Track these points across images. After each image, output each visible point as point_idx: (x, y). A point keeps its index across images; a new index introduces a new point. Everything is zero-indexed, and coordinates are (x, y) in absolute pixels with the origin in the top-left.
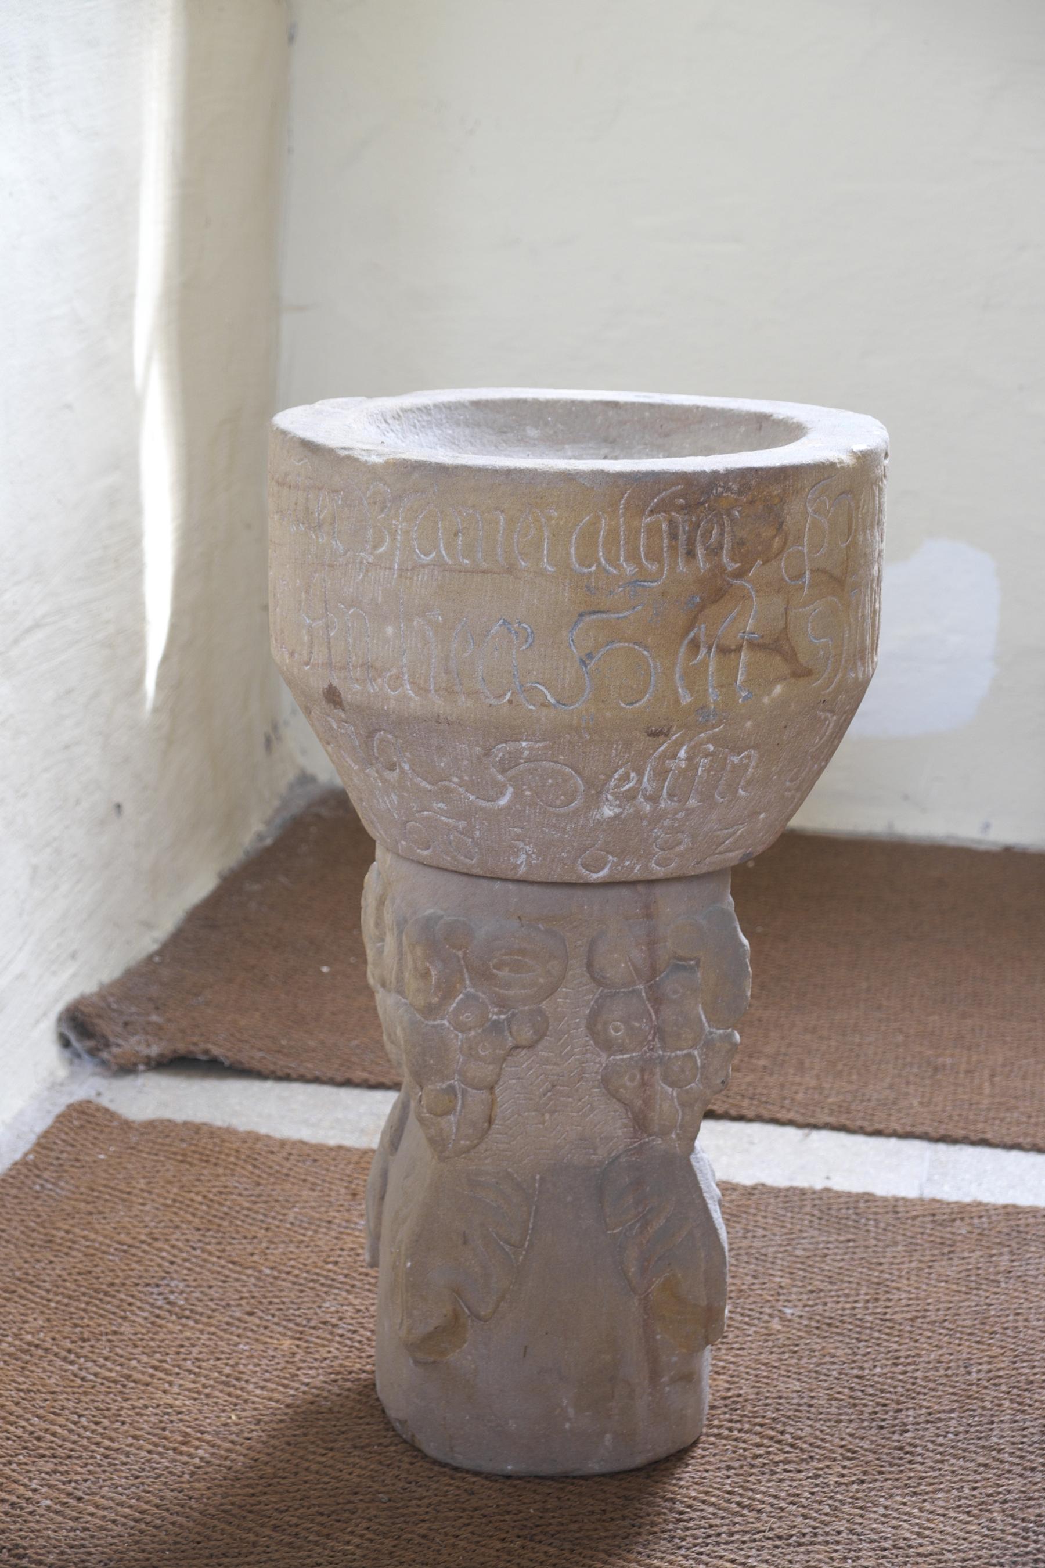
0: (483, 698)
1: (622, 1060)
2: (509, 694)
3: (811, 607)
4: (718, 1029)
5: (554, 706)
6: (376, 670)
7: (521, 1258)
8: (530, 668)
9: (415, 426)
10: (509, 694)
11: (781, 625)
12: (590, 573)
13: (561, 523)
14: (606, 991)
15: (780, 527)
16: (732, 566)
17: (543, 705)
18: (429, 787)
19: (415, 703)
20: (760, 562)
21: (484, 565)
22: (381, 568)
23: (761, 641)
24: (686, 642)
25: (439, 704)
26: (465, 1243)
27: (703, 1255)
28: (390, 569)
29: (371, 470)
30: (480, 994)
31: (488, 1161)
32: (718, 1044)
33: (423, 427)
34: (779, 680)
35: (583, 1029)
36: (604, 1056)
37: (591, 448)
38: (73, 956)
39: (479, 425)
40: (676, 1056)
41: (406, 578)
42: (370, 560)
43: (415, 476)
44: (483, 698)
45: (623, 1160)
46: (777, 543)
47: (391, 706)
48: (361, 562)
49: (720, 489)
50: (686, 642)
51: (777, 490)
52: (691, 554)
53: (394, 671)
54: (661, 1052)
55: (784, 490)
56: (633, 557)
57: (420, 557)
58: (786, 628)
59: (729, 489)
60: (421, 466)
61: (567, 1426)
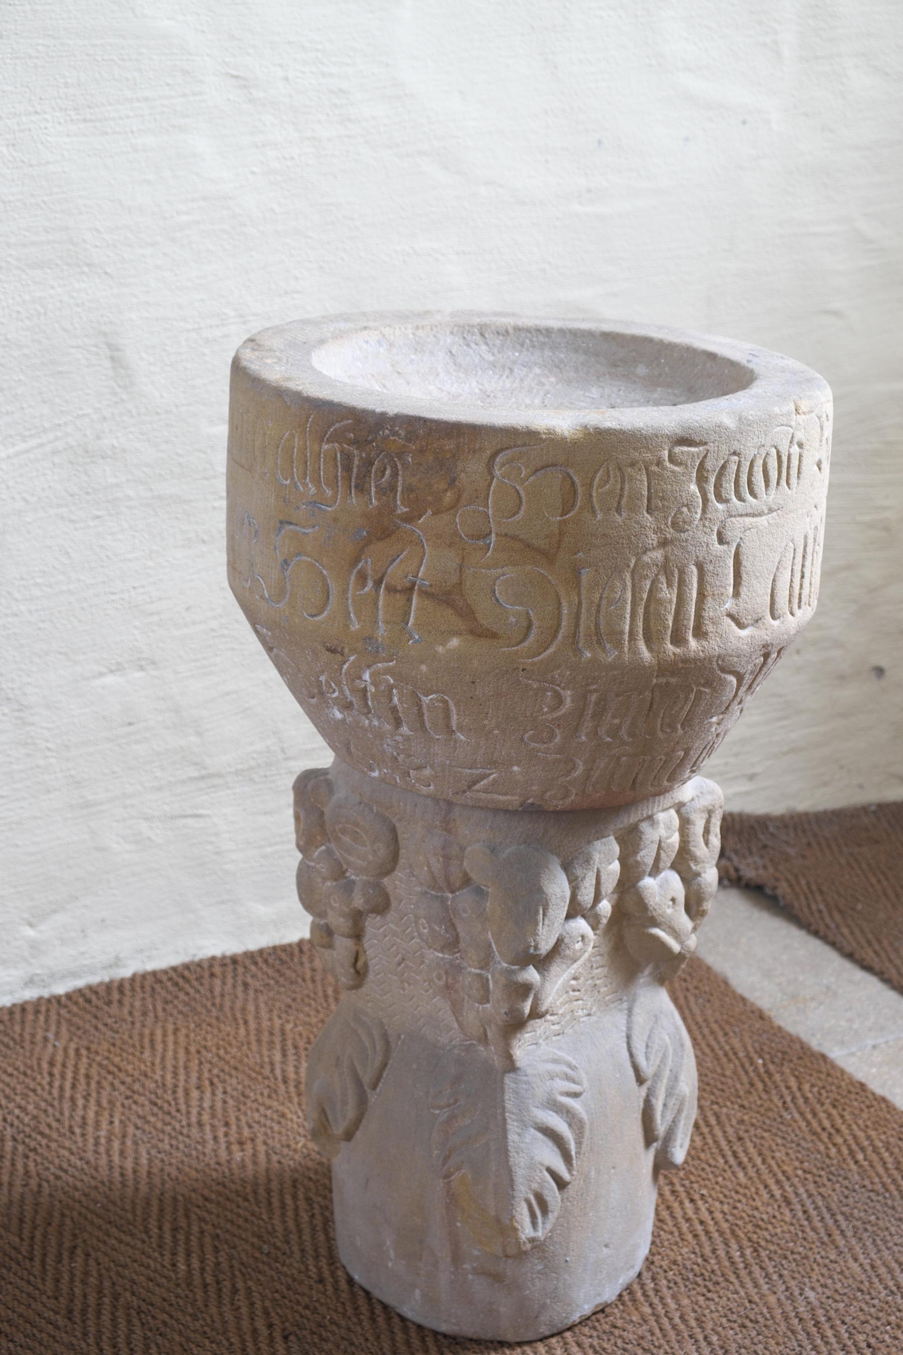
3: (500, 571)
9: (522, 345)
11: (454, 579)
15: (452, 482)
16: (402, 509)
20: (429, 512)
23: (429, 589)
24: (355, 571)
27: (494, 1169)
33: (534, 347)
34: (458, 633)
38: (751, 777)
39: (597, 355)
45: (456, 1051)
46: (449, 497)
49: (387, 432)
50: (355, 571)
51: (450, 445)
52: (362, 488)
55: (458, 447)
56: (317, 481)
58: (460, 584)
59: (396, 434)
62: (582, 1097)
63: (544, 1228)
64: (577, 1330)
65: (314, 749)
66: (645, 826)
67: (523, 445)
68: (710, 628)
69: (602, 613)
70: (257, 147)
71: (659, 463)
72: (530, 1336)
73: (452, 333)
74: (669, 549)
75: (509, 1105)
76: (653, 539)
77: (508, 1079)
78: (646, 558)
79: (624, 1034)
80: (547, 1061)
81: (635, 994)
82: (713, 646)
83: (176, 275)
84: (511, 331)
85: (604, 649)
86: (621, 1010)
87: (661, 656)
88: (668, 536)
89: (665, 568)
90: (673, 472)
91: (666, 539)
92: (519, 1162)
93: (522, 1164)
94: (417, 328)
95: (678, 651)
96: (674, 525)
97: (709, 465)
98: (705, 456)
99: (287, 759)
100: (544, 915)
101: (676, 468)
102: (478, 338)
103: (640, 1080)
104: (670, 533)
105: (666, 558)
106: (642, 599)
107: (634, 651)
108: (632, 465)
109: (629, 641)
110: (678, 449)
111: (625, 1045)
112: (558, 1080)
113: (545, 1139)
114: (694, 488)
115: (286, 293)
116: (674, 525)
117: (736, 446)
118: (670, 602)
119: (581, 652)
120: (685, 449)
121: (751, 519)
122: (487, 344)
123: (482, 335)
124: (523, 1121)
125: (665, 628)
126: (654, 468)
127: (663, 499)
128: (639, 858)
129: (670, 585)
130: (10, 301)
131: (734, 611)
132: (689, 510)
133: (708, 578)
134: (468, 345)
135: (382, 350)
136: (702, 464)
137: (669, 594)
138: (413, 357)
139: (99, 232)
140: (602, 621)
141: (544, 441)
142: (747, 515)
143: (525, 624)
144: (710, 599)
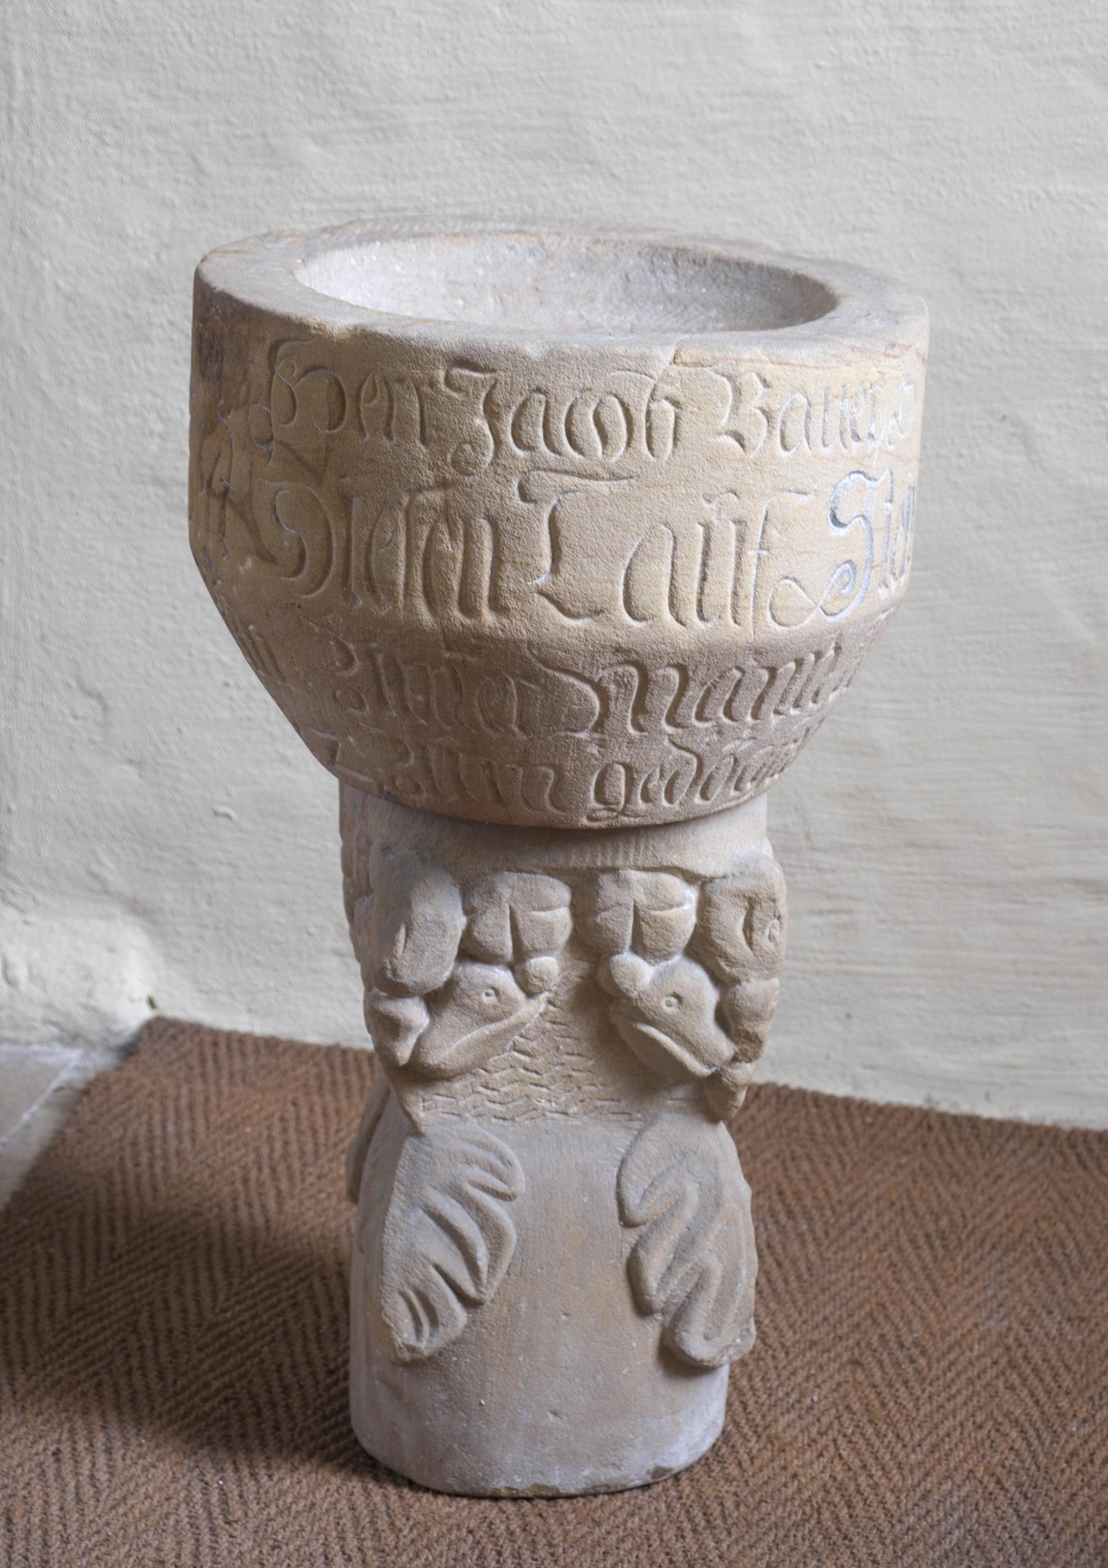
3: (278, 484)
9: (714, 280)
33: (726, 283)
62: (514, 1203)
63: (429, 1341)
64: (503, 1504)
65: (852, 846)
66: (606, 880)
67: (296, 339)
68: (512, 604)
69: (373, 556)
70: (828, 34)
71: (432, 384)
72: (435, 1484)
73: (639, 254)
74: (450, 492)
75: (401, 1173)
76: (428, 476)
77: (409, 1145)
78: (421, 498)
79: (619, 1157)
80: (471, 1142)
81: (656, 1116)
82: (518, 627)
83: (704, 188)
84: (709, 261)
85: (377, 600)
86: (627, 1128)
87: (445, 623)
88: (447, 476)
89: (446, 513)
90: (449, 398)
91: (444, 478)
92: (395, 1244)
93: (397, 1247)
94: (597, 242)
95: (467, 621)
96: (455, 463)
97: (499, 398)
98: (494, 387)
99: (813, 849)
100: (407, 936)
101: (455, 395)
102: (668, 264)
103: (627, 1222)
104: (450, 473)
105: (446, 502)
106: (418, 548)
107: (411, 609)
108: (401, 380)
109: (405, 597)
110: (456, 371)
111: (616, 1170)
112: (477, 1168)
113: (439, 1230)
114: (480, 423)
115: (854, 229)
116: (455, 463)
117: (539, 381)
118: (454, 558)
119: (355, 599)
120: (466, 372)
121: (577, 480)
122: (676, 273)
123: (675, 261)
124: (411, 1197)
125: (450, 589)
126: (426, 389)
127: (438, 428)
128: (598, 920)
129: (453, 537)
130: (493, 196)
131: (550, 589)
132: (474, 449)
133: (505, 539)
134: (653, 272)
135: (530, 261)
136: (489, 396)
137: (451, 548)
138: (573, 275)
139: (605, 122)
140: (373, 566)
141: (313, 337)
142: (566, 472)
143: (297, 552)
144: (509, 566)
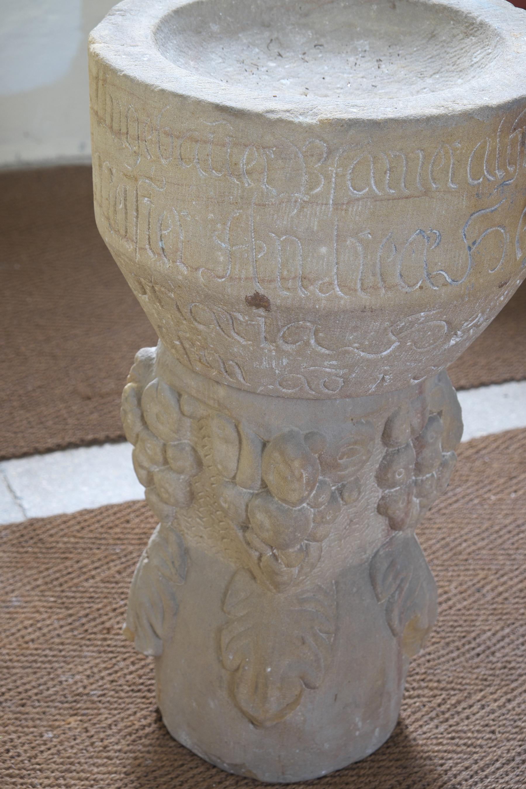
0: (400, 288)
1: (396, 491)
2: (420, 282)
4: (448, 452)
5: (450, 284)
6: (309, 280)
7: (332, 639)
8: (436, 261)
10: (420, 282)
12: (479, 184)
13: (464, 151)
14: (391, 449)
17: (444, 285)
18: (327, 352)
19: (344, 299)
21: (407, 192)
22: (317, 204)
25: (365, 299)
26: (304, 643)
28: (326, 204)
29: (309, 129)
30: (327, 479)
31: (308, 582)
32: (451, 462)
35: (373, 478)
36: (381, 491)
37: (257, 33)
40: (427, 478)
41: (342, 210)
42: (305, 199)
43: (352, 132)
44: (400, 288)
45: (381, 553)
47: (322, 305)
48: (296, 201)
53: (327, 279)
54: (414, 478)
57: (353, 193)
60: (355, 123)
61: (357, 733)
